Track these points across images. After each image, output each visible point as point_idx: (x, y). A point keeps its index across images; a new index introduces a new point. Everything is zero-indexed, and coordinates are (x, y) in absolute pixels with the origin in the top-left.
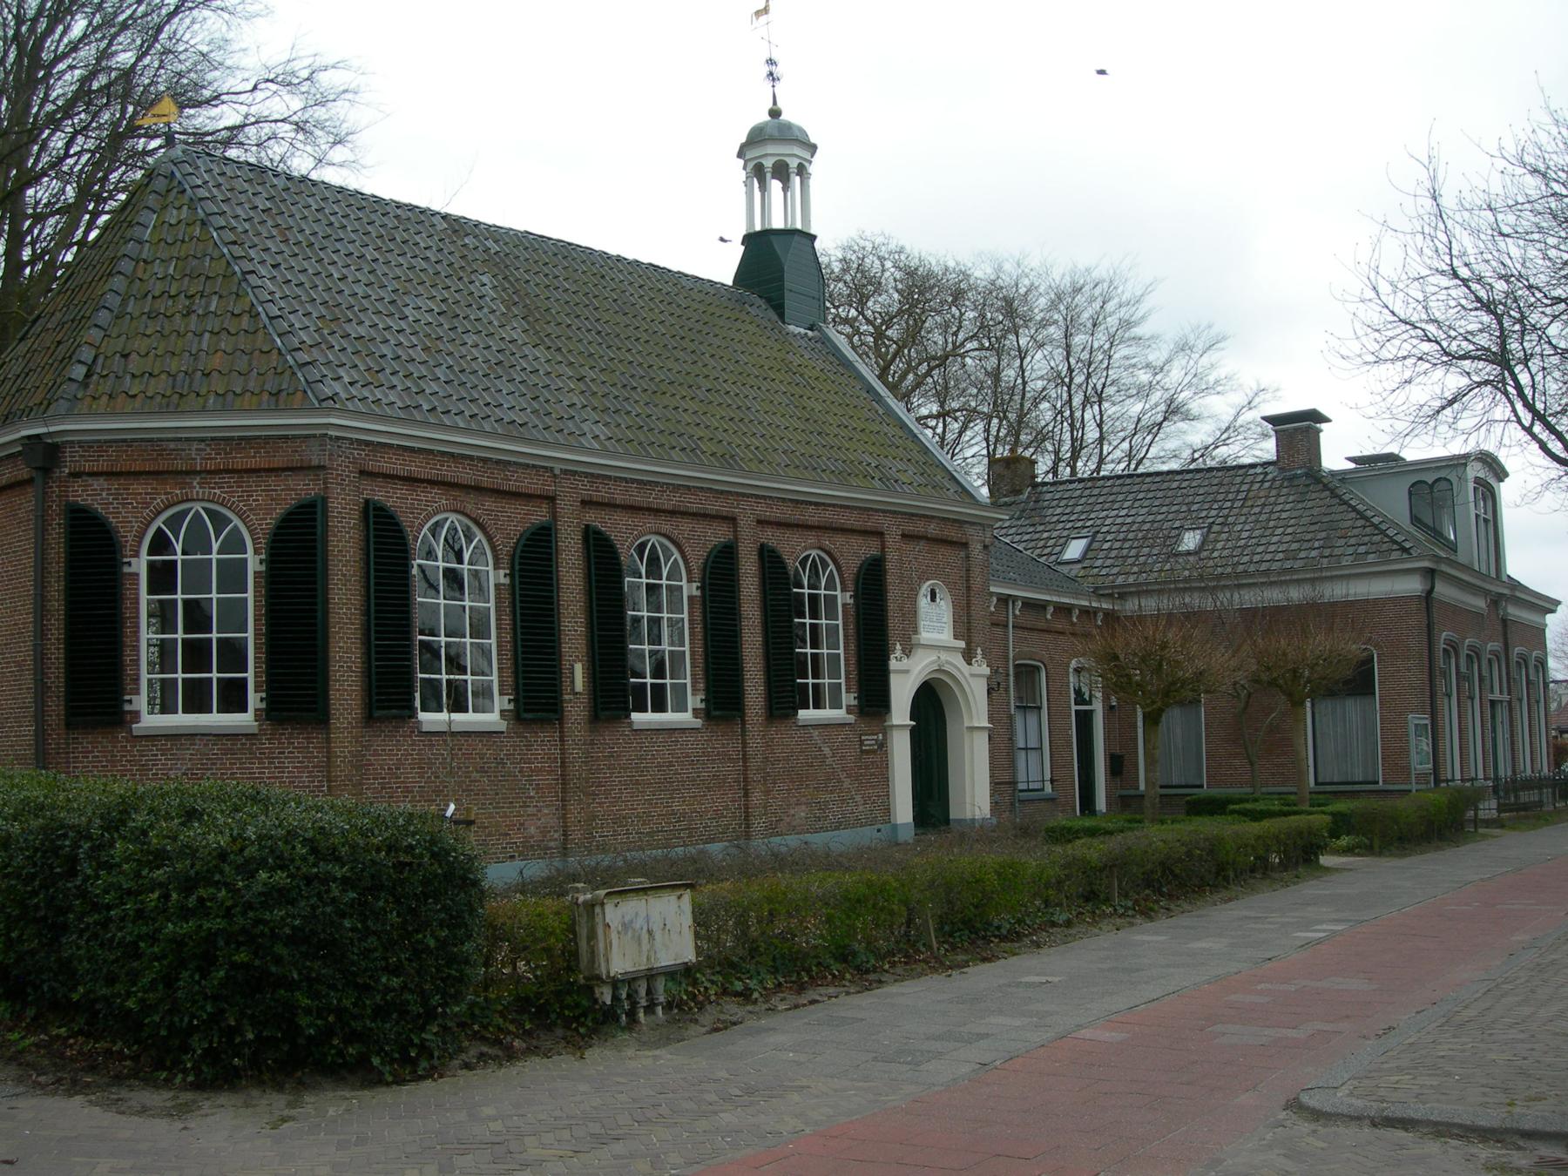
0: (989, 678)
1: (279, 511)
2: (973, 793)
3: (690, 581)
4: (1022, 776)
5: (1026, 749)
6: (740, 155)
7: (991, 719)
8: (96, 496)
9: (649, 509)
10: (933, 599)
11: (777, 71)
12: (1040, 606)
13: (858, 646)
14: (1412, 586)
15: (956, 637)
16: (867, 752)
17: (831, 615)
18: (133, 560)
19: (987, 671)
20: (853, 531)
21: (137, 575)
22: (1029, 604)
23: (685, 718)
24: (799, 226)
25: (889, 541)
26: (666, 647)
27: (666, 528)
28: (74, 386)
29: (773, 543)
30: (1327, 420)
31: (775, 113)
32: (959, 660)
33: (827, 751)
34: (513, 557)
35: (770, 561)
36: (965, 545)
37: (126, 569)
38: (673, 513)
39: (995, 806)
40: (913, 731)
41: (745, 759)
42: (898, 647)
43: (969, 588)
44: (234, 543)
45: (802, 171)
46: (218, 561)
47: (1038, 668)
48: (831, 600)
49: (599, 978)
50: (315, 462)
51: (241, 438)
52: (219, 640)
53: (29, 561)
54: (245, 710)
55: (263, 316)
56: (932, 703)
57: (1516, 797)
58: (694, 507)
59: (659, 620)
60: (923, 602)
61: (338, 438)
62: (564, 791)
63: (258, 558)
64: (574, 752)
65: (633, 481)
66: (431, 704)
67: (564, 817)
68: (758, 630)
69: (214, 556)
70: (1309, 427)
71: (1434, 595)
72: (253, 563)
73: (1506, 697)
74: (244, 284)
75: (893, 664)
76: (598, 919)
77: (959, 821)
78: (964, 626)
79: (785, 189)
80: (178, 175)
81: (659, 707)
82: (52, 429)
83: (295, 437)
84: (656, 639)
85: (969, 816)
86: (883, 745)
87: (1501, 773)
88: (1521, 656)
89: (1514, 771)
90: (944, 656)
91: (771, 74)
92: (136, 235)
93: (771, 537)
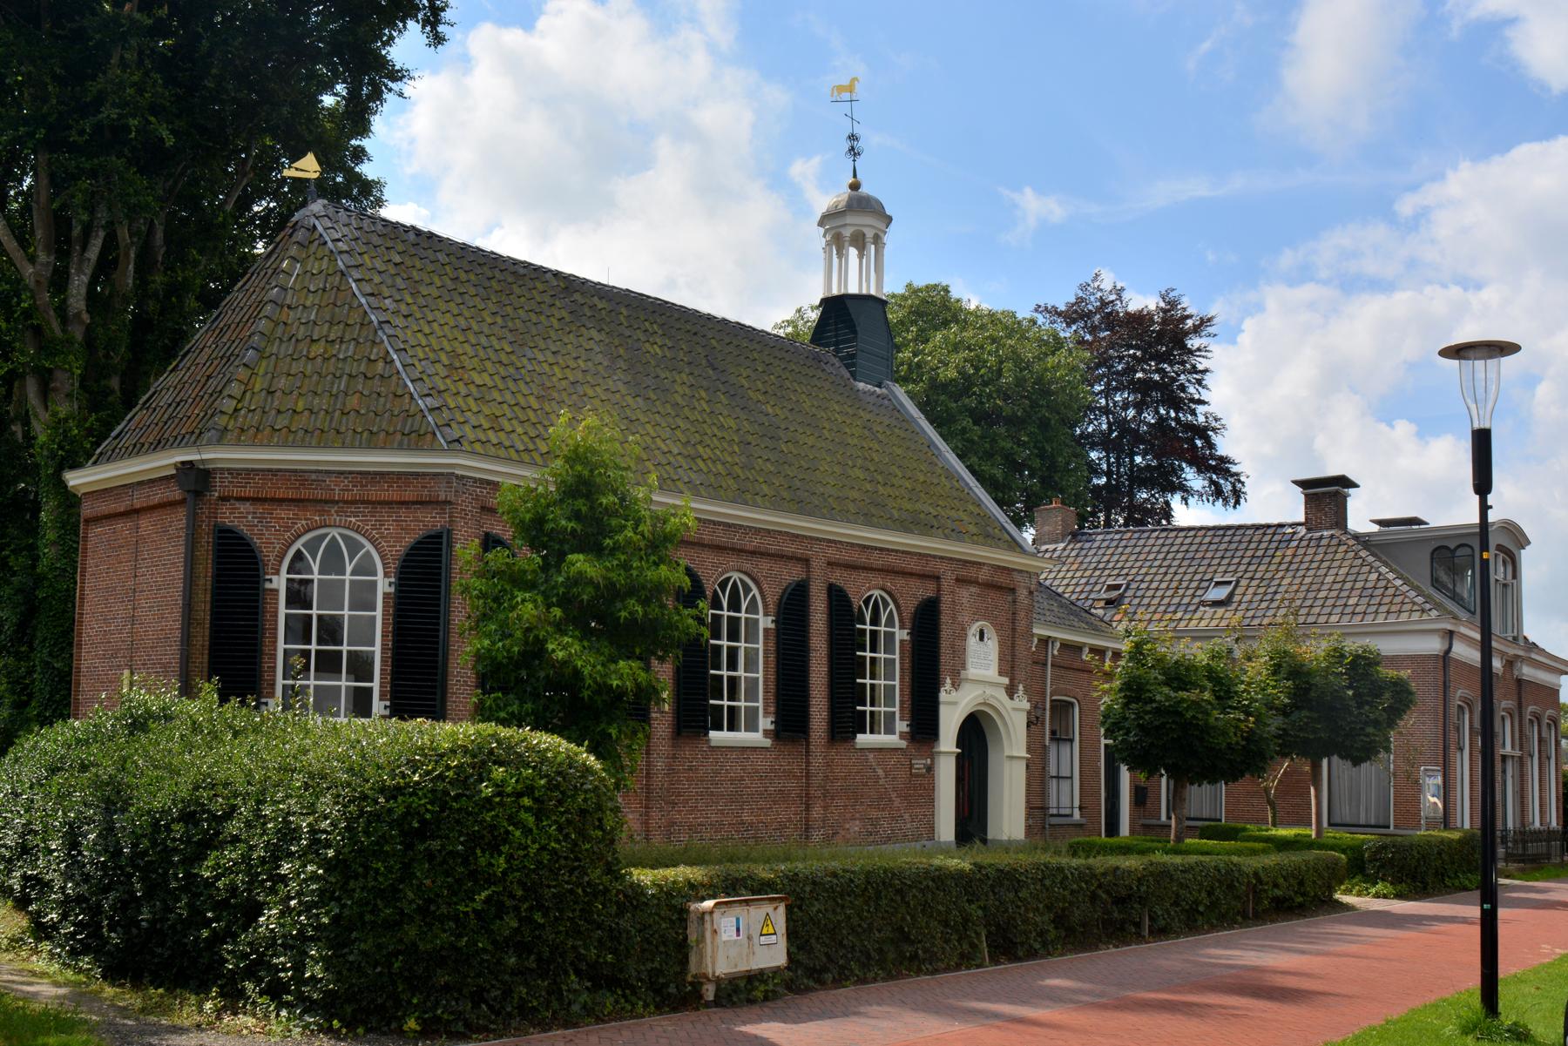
0: (1029, 713)
1: (410, 539)
2: (1009, 817)
3: (766, 614)
4: (1053, 802)
5: (1058, 777)
6: (821, 223)
7: (1029, 751)
8: (239, 518)
9: (733, 549)
10: (982, 638)
11: (859, 145)
12: (1077, 648)
13: (913, 680)
14: (1434, 645)
15: (1001, 674)
16: (917, 776)
17: (889, 649)
18: (274, 578)
19: (1027, 706)
20: (911, 574)
21: (277, 591)
22: (1066, 646)
23: (756, 738)
24: (873, 292)
25: (944, 583)
26: (741, 673)
27: (747, 566)
28: (226, 418)
29: (840, 583)
30: (1355, 486)
31: (855, 186)
32: (1002, 695)
33: (880, 772)
34: (779, 604)
35: (838, 598)
36: (1013, 590)
37: (268, 586)
38: (753, 553)
39: (1029, 829)
40: (959, 757)
41: (808, 776)
42: (948, 681)
43: (1014, 630)
44: (365, 568)
45: (877, 240)
46: (352, 582)
47: (1072, 704)
48: (890, 637)
49: (705, 976)
50: (442, 497)
51: (376, 473)
52: (349, 652)
53: (178, 574)
54: (756, 730)
55: (398, 364)
56: (976, 731)
57: (1524, 848)
58: (773, 548)
59: (736, 648)
60: (972, 641)
61: (463, 477)
62: (648, 798)
63: (387, 581)
64: (660, 764)
65: (720, 523)
66: (718, 727)
67: (646, 823)
68: (825, 661)
69: (348, 577)
70: (1337, 492)
71: (1452, 655)
72: (383, 585)
73: (1518, 753)
74: (380, 333)
75: (943, 696)
76: (708, 925)
77: (994, 841)
78: (1008, 665)
79: (861, 256)
80: (320, 229)
81: (732, 727)
82: (205, 457)
83: (424, 474)
84: (733, 665)
85: (1005, 838)
86: (930, 769)
87: (1510, 825)
88: (1534, 714)
89: (1523, 824)
90: (989, 691)
91: (852, 149)
92: (281, 282)
93: (838, 577)
